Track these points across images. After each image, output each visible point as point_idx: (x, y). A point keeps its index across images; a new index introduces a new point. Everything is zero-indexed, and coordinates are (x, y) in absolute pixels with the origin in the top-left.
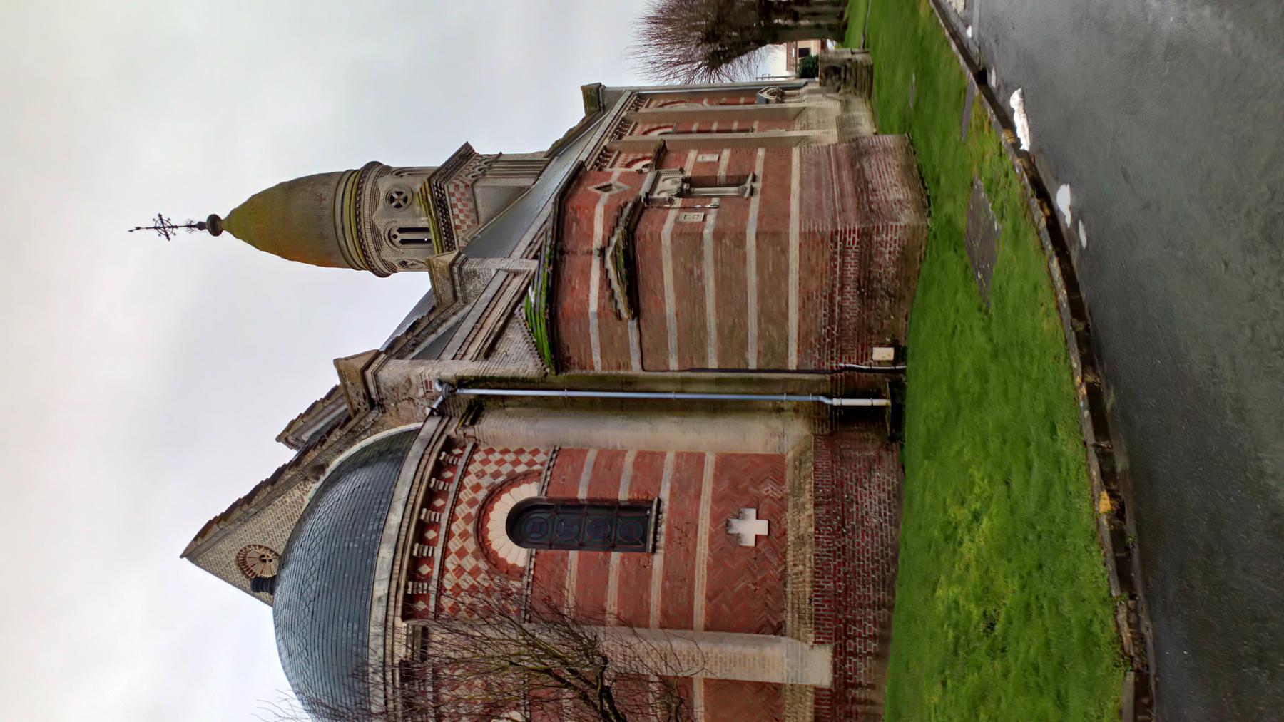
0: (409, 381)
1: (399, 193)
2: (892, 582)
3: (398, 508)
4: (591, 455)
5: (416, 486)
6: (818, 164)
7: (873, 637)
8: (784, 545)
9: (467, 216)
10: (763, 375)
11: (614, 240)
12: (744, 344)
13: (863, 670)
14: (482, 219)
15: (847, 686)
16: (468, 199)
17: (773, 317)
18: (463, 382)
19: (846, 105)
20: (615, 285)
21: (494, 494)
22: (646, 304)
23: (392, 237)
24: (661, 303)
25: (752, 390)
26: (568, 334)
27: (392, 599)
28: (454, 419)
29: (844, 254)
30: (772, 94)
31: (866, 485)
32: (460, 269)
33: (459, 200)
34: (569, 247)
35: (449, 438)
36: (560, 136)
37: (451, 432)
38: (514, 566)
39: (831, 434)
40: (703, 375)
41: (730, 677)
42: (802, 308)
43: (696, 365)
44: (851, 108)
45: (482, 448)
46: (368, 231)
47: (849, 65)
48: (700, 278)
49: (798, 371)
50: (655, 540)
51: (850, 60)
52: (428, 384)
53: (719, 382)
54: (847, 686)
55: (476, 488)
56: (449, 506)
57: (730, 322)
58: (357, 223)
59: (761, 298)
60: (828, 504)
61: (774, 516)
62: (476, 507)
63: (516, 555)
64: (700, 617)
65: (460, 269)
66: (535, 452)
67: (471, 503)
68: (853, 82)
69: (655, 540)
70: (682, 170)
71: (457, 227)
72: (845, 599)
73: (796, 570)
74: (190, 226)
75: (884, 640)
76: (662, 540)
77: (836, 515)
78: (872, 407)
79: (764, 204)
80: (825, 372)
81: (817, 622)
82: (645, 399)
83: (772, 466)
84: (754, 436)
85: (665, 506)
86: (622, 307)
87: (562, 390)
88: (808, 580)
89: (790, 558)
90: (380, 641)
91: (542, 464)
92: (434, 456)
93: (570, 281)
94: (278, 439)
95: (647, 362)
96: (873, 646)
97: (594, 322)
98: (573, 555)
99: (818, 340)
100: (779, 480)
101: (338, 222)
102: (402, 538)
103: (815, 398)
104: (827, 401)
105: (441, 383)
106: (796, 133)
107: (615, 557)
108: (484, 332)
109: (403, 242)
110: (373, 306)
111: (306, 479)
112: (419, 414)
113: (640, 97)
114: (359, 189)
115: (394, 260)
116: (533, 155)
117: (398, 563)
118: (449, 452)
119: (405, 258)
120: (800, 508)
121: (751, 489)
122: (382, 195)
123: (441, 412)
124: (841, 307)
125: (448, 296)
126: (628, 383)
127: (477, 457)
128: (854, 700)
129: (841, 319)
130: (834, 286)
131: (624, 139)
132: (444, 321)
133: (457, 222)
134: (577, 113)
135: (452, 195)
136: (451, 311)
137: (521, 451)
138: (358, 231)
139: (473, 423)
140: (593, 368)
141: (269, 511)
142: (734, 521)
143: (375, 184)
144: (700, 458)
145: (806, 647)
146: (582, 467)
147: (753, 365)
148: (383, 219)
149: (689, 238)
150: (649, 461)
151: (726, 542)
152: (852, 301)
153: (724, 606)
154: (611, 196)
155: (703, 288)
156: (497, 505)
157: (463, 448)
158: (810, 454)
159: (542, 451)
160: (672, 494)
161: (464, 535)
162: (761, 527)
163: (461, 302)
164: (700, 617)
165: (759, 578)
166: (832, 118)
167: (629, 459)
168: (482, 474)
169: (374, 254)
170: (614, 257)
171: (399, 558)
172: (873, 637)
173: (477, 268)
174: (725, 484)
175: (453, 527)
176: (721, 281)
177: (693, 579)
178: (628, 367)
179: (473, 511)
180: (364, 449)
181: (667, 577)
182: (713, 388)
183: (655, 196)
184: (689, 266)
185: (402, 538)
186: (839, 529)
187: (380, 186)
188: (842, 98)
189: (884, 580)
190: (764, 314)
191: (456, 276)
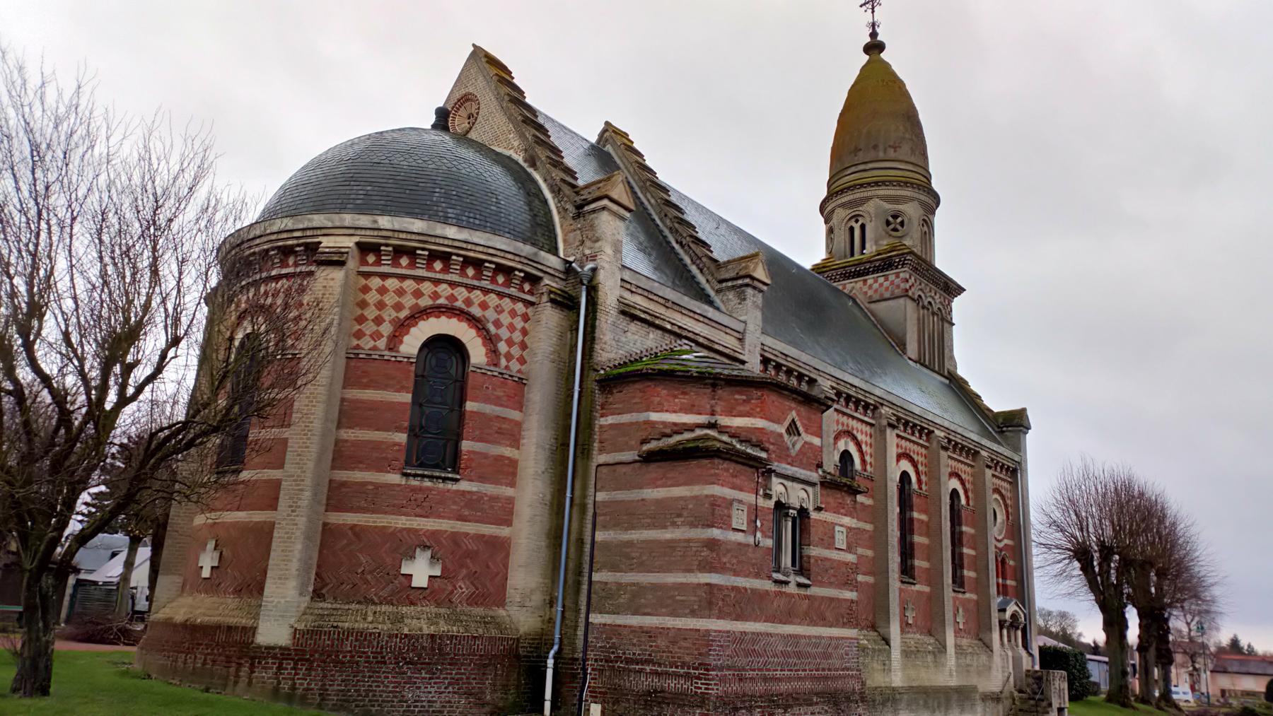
0: (597, 240)
1: (902, 224)
2: (345, 709)
3: (464, 235)
4: (515, 415)
5: (485, 250)
6: (827, 656)
7: (293, 688)
8: (400, 603)
9: (876, 291)
10: (585, 587)
11: (725, 438)
12: (614, 568)
13: (265, 675)
14: (873, 306)
15: (253, 658)
16: (893, 293)
17: (637, 600)
18: (593, 290)
19: (996, 698)
20: (677, 438)
21: (476, 323)
22: (654, 469)
23: (856, 218)
24: (654, 484)
25: (570, 575)
26: (633, 392)
27: (289, 235)
28: (563, 283)
29: (688, 676)
30: (1014, 616)
31: (450, 689)
32: (747, 285)
33: (892, 283)
34: (720, 392)
35: (541, 279)
36: (975, 386)
37: (547, 281)
38: (401, 342)
39: (517, 657)
40: (589, 526)
41: (274, 544)
42: (642, 630)
43: (599, 519)
44: (989, 703)
45: (530, 311)
46: (862, 195)
47: (1044, 704)
48: (674, 524)
49: (587, 623)
50: (415, 476)
51: (1050, 705)
52: (593, 258)
53: (581, 542)
54: (253, 658)
55: (484, 306)
56: (465, 281)
57: (634, 555)
58: (869, 184)
59: (655, 587)
60: (433, 649)
61: (431, 593)
62: (463, 306)
63: (412, 344)
64: (336, 518)
65: (747, 285)
66: (522, 361)
67: (468, 302)
68: (1025, 707)
69: (415, 476)
70: (819, 509)
71: (865, 281)
72: (333, 661)
73: (370, 613)
74: (873, 25)
75: (290, 698)
76: (414, 482)
77: (420, 657)
78: (544, 700)
79: (762, 596)
80: (585, 652)
81: (314, 633)
82: (567, 468)
83: (491, 590)
84: (525, 578)
85: (455, 487)
86: (653, 445)
87: (580, 386)
88: (356, 625)
89: (384, 608)
90: (338, 224)
91: (507, 368)
92: (519, 266)
93: (684, 393)
94: (607, 123)
95: (604, 470)
96: (285, 686)
97: (641, 417)
98: (407, 397)
99: (613, 646)
100: (473, 600)
101: (871, 166)
102: (433, 240)
103: (557, 640)
104: (552, 653)
105: (594, 270)
106: (950, 639)
107: (402, 438)
108: (660, 310)
109: (852, 229)
110: (776, 204)
111: (526, 150)
112: (571, 251)
113: (1013, 472)
114: (919, 187)
115: (835, 221)
116: (952, 358)
117: (409, 237)
118: (524, 279)
119: (836, 231)
120: (431, 622)
121: (464, 572)
122: (900, 207)
123: (569, 270)
124: (640, 671)
125: (725, 274)
126: (584, 451)
127: (520, 307)
128: (240, 665)
129: (630, 671)
130: (660, 665)
131: (943, 453)
132: (701, 271)
133: (870, 282)
134: (996, 403)
135: (897, 275)
136: (710, 278)
137: (524, 346)
138: (861, 185)
139: (552, 301)
140: (602, 416)
141: (504, 119)
142: (429, 553)
143: (912, 199)
144: (508, 523)
145: (292, 621)
146: (502, 405)
147: (596, 577)
148: (874, 208)
149: (716, 513)
150: (507, 471)
151: (408, 545)
152: (645, 683)
153: (345, 542)
154: (781, 435)
155: (665, 527)
156: (464, 325)
157: (531, 293)
158: (494, 632)
159: (523, 367)
160: (464, 493)
161: (436, 296)
162: (420, 581)
163: (719, 286)
164: (336, 518)
165: (369, 577)
166: (974, 680)
167: (508, 452)
168: (499, 310)
169: (840, 202)
170: (706, 438)
171: (413, 237)
172: (293, 688)
173: (749, 302)
174: (473, 546)
175: (444, 286)
176: (671, 545)
177: (373, 512)
178: (601, 451)
179: (459, 304)
180: (545, 202)
181: (377, 486)
182: (574, 536)
183: (775, 480)
184: (685, 514)
185: (433, 240)
186: (404, 659)
187: (910, 204)
188: (1006, 694)
189: (347, 701)
190: (640, 590)
191: (740, 282)
